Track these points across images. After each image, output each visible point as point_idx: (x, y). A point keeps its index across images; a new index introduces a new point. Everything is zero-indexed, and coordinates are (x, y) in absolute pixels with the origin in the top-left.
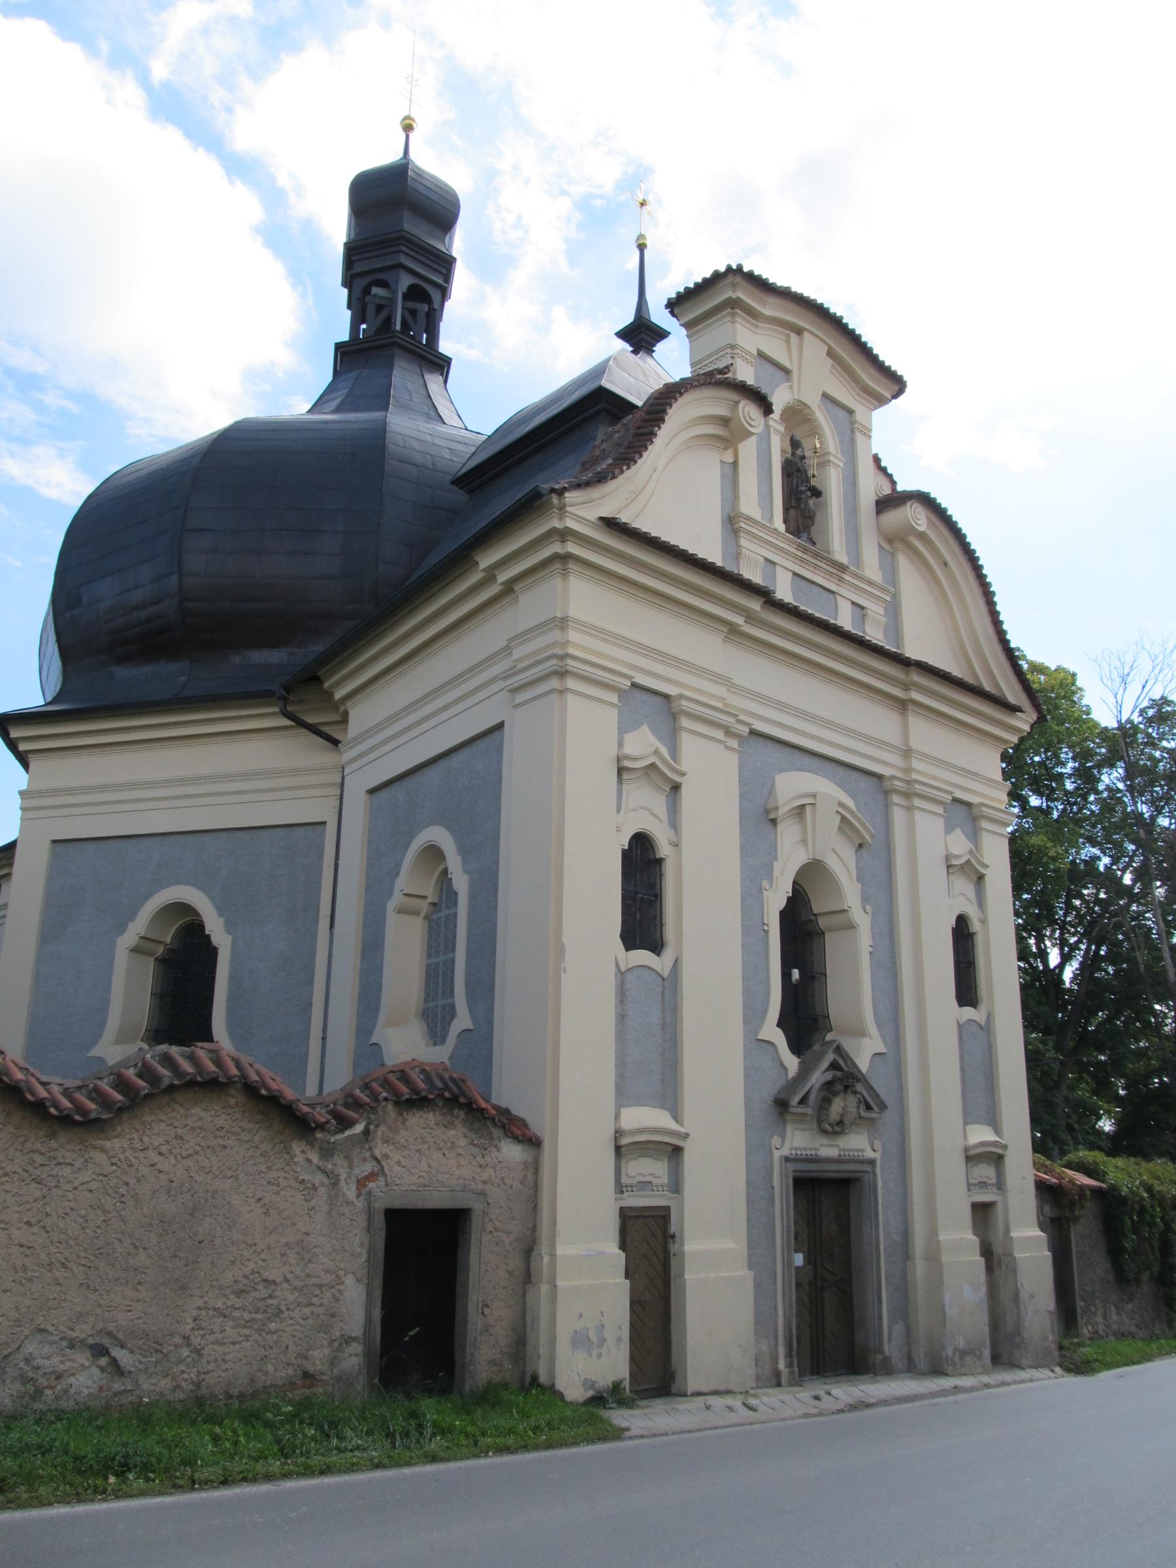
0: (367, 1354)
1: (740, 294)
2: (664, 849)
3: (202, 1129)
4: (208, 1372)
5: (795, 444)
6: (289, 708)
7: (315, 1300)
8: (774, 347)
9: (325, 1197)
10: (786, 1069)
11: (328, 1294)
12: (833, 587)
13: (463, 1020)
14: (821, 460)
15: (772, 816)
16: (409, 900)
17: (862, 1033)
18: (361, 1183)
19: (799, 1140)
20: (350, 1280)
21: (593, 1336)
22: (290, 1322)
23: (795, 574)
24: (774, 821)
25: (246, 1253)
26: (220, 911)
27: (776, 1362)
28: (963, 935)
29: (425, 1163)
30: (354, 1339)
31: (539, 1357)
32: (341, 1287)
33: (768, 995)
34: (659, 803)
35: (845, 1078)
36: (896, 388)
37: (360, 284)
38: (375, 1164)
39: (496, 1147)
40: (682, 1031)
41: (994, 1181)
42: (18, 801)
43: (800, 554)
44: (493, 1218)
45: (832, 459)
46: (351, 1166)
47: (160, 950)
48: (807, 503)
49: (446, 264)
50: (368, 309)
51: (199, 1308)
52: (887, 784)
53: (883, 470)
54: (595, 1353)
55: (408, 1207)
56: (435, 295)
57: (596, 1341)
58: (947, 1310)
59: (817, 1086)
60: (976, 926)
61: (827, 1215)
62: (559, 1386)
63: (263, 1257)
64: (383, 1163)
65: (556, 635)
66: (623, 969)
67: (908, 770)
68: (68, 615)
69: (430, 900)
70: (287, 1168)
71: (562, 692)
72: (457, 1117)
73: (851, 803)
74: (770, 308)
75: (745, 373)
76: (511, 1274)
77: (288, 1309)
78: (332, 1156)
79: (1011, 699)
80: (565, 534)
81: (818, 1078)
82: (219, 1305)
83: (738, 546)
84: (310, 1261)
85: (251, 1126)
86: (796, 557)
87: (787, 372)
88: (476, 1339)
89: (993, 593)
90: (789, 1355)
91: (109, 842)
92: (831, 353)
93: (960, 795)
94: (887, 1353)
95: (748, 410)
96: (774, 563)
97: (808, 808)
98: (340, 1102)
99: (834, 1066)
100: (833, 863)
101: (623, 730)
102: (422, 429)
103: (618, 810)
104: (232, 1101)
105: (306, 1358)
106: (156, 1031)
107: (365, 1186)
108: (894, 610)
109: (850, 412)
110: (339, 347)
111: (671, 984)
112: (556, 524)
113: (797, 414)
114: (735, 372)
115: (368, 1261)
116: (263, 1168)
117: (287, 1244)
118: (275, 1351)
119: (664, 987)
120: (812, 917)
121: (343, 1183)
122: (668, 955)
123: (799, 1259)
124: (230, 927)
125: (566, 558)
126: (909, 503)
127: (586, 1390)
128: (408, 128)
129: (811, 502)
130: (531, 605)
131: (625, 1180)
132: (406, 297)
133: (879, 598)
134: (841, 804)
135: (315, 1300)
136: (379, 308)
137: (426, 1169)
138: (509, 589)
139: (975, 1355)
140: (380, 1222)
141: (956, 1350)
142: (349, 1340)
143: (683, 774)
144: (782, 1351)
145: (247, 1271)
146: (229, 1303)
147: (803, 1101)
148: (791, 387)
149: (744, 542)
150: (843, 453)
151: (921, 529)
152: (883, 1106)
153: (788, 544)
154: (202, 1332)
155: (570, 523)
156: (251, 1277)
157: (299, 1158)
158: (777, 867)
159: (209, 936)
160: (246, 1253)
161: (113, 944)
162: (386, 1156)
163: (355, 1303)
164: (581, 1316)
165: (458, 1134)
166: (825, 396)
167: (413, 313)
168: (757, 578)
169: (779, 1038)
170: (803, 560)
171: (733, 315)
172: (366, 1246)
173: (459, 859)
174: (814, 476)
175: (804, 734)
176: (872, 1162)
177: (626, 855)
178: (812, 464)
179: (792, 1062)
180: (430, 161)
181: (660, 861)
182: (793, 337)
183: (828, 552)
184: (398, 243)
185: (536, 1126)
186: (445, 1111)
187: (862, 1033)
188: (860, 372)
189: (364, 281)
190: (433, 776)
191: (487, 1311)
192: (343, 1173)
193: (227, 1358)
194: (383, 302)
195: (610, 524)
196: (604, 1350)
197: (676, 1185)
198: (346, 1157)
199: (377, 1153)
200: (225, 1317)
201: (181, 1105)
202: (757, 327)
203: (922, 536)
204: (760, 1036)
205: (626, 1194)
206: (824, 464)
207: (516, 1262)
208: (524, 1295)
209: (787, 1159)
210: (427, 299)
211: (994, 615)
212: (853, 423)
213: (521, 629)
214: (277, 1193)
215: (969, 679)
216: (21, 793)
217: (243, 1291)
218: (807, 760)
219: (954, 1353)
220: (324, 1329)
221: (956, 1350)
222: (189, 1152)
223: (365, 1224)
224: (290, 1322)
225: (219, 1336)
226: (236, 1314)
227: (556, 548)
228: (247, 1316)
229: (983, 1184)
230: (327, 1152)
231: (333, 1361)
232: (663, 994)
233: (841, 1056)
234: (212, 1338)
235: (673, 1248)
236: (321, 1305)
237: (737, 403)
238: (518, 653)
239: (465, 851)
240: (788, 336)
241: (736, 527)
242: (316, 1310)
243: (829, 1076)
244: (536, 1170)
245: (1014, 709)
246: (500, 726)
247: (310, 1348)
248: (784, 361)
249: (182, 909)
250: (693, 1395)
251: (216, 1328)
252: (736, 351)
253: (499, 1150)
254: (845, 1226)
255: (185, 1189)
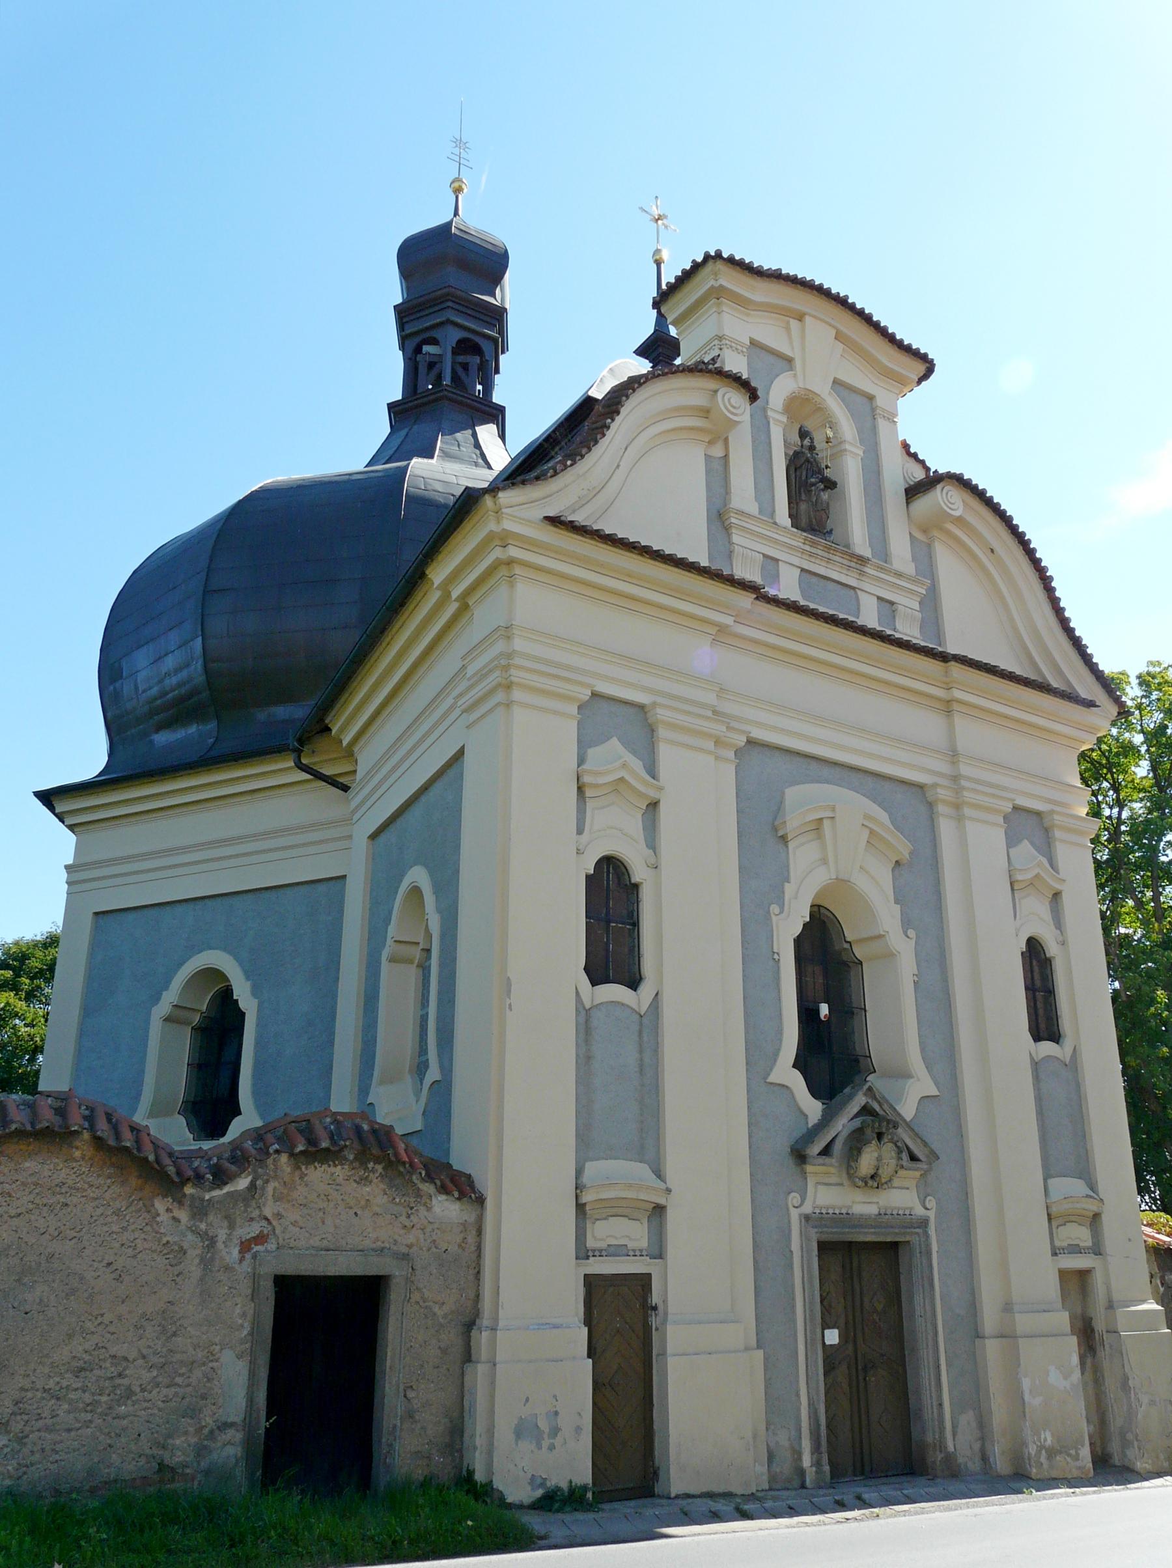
0: (248, 1443)
1: (723, 282)
2: (639, 873)
3: (36, 1184)
4: (32, 1465)
5: (803, 434)
6: (304, 761)
7: (179, 1380)
8: (770, 333)
9: (197, 1261)
10: (806, 1116)
11: (198, 1373)
12: (852, 582)
13: (433, 1074)
14: (835, 450)
15: (780, 833)
16: (402, 947)
17: (906, 1075)
18: (245, 1246)
19: (827, 1193)
20: (227, 1356)
21: (543, 1425)
22: (145, 1405)
23: (803, 570)
24: (784, 839)
25: (88, 1324)
26: (248, 975)
27: (800, 1458)
28: (1036, 960)
29: (329, 1221)
30: (232, 1425)
31: (475, 1448)
32: (214, 1364)
33: (779, 1032)
34: (634, 824)
35: (877, 1124)
36: (921, 368)
37: (412, 344)
38: (264, 1223)
39: (425, 1205)
40: (663, 1071)
41: (1089, 1243)
42: (64, 875)
43: (807, 548)
44: (421, 1286)
45: (848, 447)
46: (232, 1226)
47: (197, 1018)
48: (818, 497)
49: (497, 316)
50: (420, 367)
51: (22, 1389)
52: (930, 795)
53: (914, 456)
54: (545, 1443)
55: (303, 1273)
56: (486, 347)
57: (547, 1431)
58: (1027, 1397)
59: (845, 1134)
60: (1052, 949)
61: (867, 1288)
62: (498, 1484)
63: (112, 1329)
64: (274, 1223)
65: (500, 646)
66: (588, 1007)
67: (955, 778)
68: (112, 688)
69: (421, 946)
70: (148, 1228)
71: (508, 705)
72: (373, 1171)
73: (883, 816)
74: (760, 292)
75: (735, 363)
76: (444, 1351)
77: (143, 1390)
78: (206, 1214)
79: (1084, 694)
80: (505, 539)
81: (843, 1125)
82: (51, 1384)
83: (731, 543)
84: (175, 1334)
85: (101, 1181)
86: (803, 551)
87: (789, 361)
88: (395, 1426)
89: (1051, 578)
90: (816, 1449)
91: (145, 911)
92: (839, 336)
93: (1022, 802)
94: (951, 1448)
95: (732, 400)
96: (777, 560)
97: (826, 823)
98: (226, 1155)
99: (866, 1110)
100: (862, 883)
101: (584, 745)
102: (448, 471)
103: (580, 831)
104: (77, 1154)
105: (164, 1447)
106: (194, 1103)
107: (249, 1249)
108: (931, 602)
109: (871, 398)
110: (391, 407)
111: (649, 1024)
112: (492, 526)
113: (802, 405)
114: (723, 362)
115: (251, 1334)
116: (115, 1228)
117: (144, 1314)
118: (123, 1440)
119: (641, 1024)
120: (846, 946)
121: (220, 1245)
122: (647, 990)
123: (832, 1337)
124: (256, 991)
125: (510, 562)
126: (939, 487)
127: (533, 1489)
128: (458, 191)
129: (825, 496)
130: (485, 616)
131: (591, 1243)
132: (455, 352)
133: (912, 592)
134: (867, 817)
135: (179, 1380)
136: (431, 366)
137: (332, 1230)
138: (464, 607)
139: (1069, 1455)
140: (268, 1291)
141: (1041, 1448)
142: (224, 1426)
143: (661, 789)
144: (806, 1445)
145: (88, 1345)
146: (64, 1383)
147: (826, 1151)
148: (795, 376)
149: (735, 539)
150: (862, 441)
151: (957, 513)
152: (934, 1156)
153: (797, 539)
154: (26, 1417)
155: (508, 525)
156: (96, 1353)
157: (164, 1217)
158: (789, 889)
159: (237, 1001)
160: (88, 1324)
161: (149, 1014)
162: (279, 1216)
163: (235, 1384)
164: (527, 1400)
165: (375, 1191)
166: (836, 382)
167: (465, 367)
168: (752, 575)
169: (797, 1082)
170: (811, 555)
171: (719, 305)
172: (249, 1317)
173: (434, 898)
174: (827, 467)
175: (842, 748)
176: (924, 1223)
177: (591, 881)
178: (823, 453)
179: (813, 1108)
180: (481, 220)
181: (636, 886)
182: (794, 324)
183: (848, 546)
184: (450, 304)
185: (486, 1183)
186: (356, 1164)
187: (906, 1075)
188: (873, 352)
189: (417, 340)
190: (417, 811)
191: (411, 1394)
192: (222, 1234)
193: (58, 1447)
194: (435, 359)
195: (554, 521)
196: (558, 1441)
197: (658, 1252)
198: (227, 1217)
199: (268, 1212)
200: (58, 1399)
201: (11, 1158)
202: (748, 315)
203: (959, 521)
204: (771, 1079)
205: (592, 1259)
206: (839, 453)
207: (451, 1337)
208: (463, 1374)
209: (807, 1218)
210: (477, 350)
211: (1054, 602)
212: (873, 410)
213: (475, 641)
214: (134, 1257)
215: (1032, 676)
216: (66, 867)
217: (82, 1369)
218: (826, 771)
219: (1039, 1452)
220: (192, 1412)
221: (1041, 1448)
222: (19, 1211)
223: (249, 1291)
224: (145, 1405)
225: (49, 1422)
226: (72, 1396)
227: (497, 553)
228: (87, 1398)
229: (1075, 1250)
230: (200, 1210)
231: (201, 1451)
232: (640, 1032)
233: (875, 1098)
234: (41, 1423)
235: (654, 1321)
236: (189, 1385)
237: (716, 391)
238: (470, 671)
239: (438, 889)
240: (788, 322)
241: (727, 523)
242: (181, 1391)
243: (857, 1123)
244: (480, 1232)
245: (1091, 704)
246: (461, 752)
247: (170, 1436)
248: (785, 349)
249: (213, 974)
250: (677, 1497)
251: (46, 1413)
252: (724, 342)
253: (429, 1209)
254: (895, 1298)
255: (12, 1253)
